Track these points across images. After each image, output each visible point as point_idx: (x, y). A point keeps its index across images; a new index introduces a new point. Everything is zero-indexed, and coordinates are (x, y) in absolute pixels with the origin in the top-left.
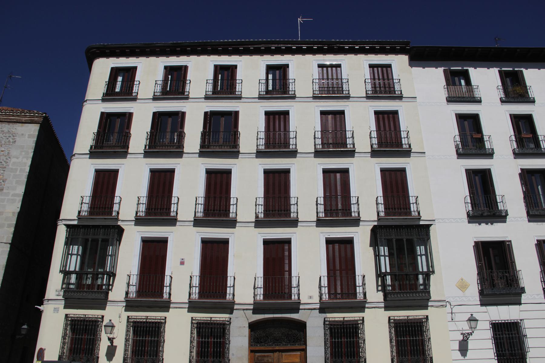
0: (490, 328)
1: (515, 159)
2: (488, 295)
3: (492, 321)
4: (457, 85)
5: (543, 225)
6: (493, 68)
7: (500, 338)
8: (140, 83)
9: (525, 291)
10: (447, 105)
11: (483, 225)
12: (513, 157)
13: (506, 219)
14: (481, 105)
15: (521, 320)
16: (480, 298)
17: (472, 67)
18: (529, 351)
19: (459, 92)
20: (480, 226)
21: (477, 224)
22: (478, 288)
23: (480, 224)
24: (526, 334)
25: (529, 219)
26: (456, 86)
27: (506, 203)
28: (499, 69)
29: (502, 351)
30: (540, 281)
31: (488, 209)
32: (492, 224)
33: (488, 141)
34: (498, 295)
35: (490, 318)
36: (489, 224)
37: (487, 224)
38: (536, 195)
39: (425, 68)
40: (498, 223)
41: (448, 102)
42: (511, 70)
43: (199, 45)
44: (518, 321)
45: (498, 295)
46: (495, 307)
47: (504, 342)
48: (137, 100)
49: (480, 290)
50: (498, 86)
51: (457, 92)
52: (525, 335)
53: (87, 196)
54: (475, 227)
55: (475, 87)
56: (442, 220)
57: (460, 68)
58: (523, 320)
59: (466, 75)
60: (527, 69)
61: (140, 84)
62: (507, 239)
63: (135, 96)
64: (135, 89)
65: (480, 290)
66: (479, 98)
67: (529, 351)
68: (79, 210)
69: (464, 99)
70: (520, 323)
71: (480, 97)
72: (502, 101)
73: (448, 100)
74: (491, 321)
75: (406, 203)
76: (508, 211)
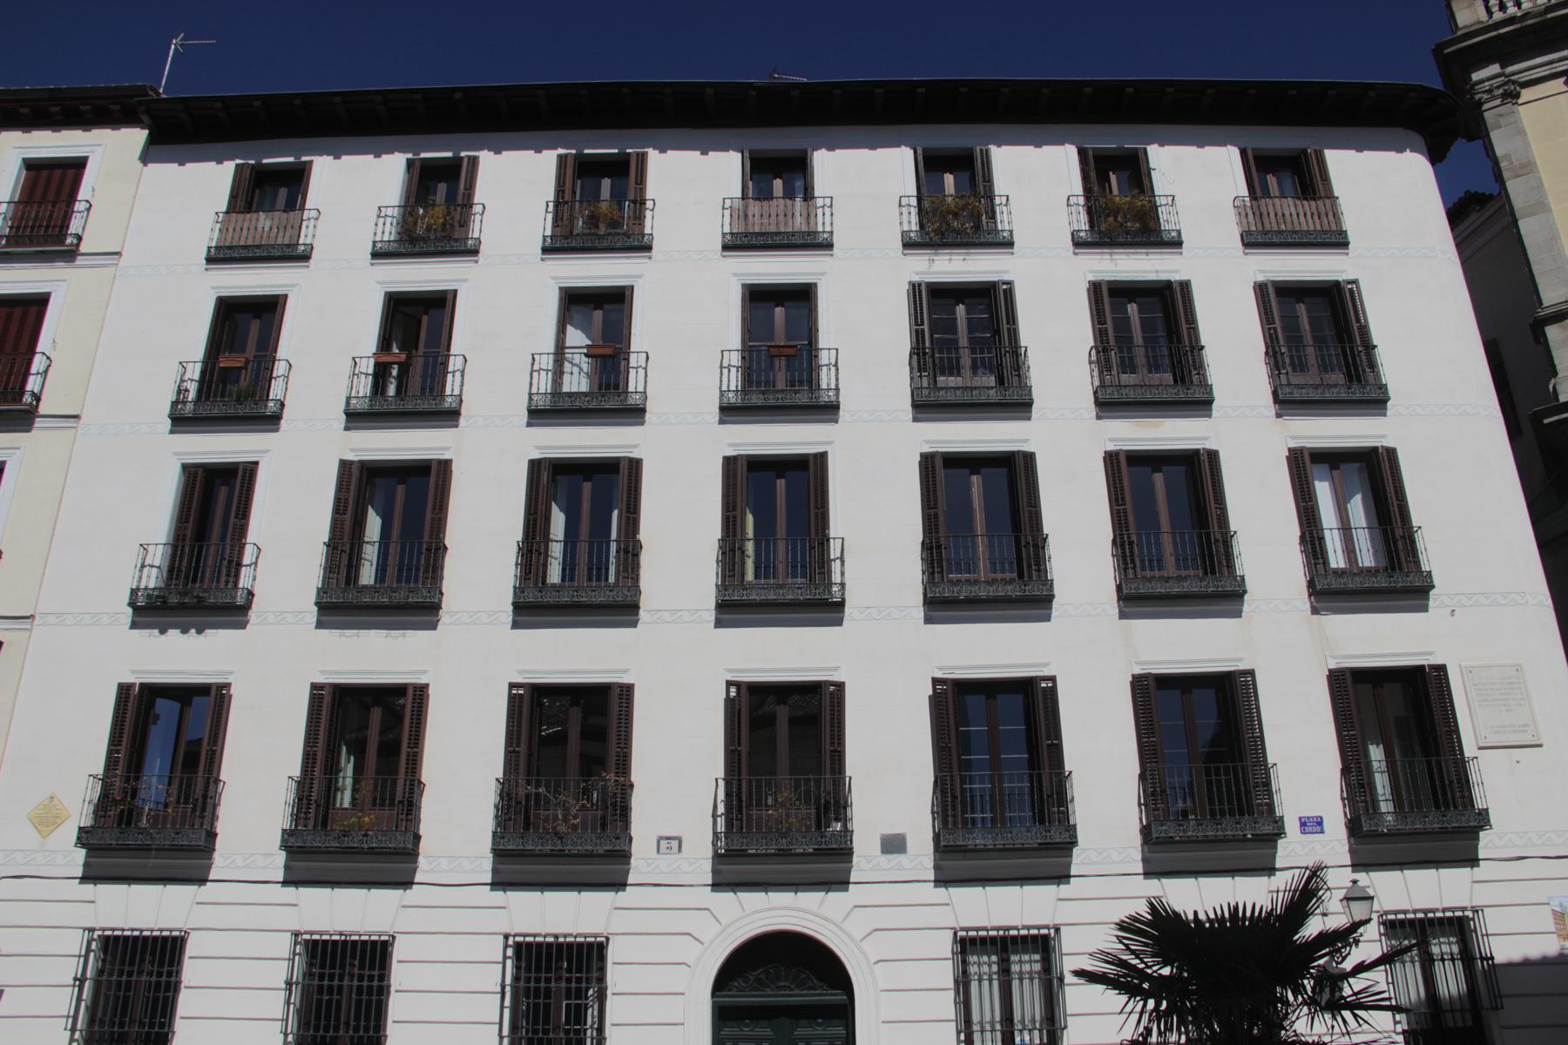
0: (1381, 935)
1: (1101, 421)
2: (1169, 841)
3: (1386, 913)
4: (1272, 195)
5: (358, 636)
6: (1063, 144)
7: (330, 988)
8: (91, 205)
9: (1489, 821)
10: (1243, 256)
11: (174, 633)
12: (1274, 412)
13: (1428, 599)
14: (308, 267)
15: (1475, 911)
16: (1143, 851)
17: (328, 155)
18: (1502, 1007)
19: (1295, 216)
20: (163, 636)
21: (156, 632)
22: (1141, 819)
23: (163, 632)
24: (1491, 954)
25: (1314, 604)
26: (1270, 197)
27: (1426, 550)
28: (410, 156)
29: (367, 1029)
30: (1339, 797)
31: (1201, 575)
32: (200, 632)
33: (640, 370)
34: (1451, 832)
35: (1411, 905)
36: (193, 631)
37: (185, 631)
38: (422, 542)
39: (666, 152)
40: (220, 631)
41: (1076, 248)
42: (449, 158)
43: (55, 96)
44: (1466, 913)
45: (1451, 832)
46: (1398, 873)
47: (339, 1003)
48: (79, 257)
49: (1349, 820)
50: (1235, 198)
51: (1302, 217)
52: (1489, 955)
53: (157, 544)
54: (149, 638)
55: (1163, 201)
56: (1469, 599)
57: (291, 159)
58: (1480, 912)
59: (1135, 170)
60: (999, 146)
61: (92, 209)
62: (1242, 666)
63: (72, 244)
64: (75, 226)
65: (1349, 820)
66: (1174, 234)
67: (1499, 1006)
68: (134, 587)
69: (256, 253)
70: (1473, 919)
71: (1178, 228)
72: (1079, 244)
73: (1246, 241)
74: (1382, 916)
75: (823, 558)
76: (1433, 574)
